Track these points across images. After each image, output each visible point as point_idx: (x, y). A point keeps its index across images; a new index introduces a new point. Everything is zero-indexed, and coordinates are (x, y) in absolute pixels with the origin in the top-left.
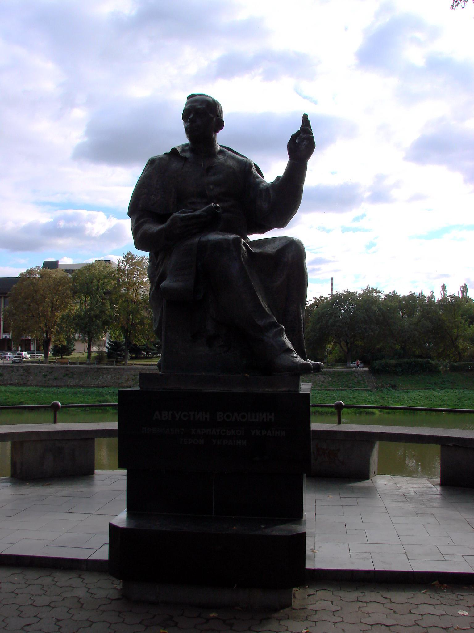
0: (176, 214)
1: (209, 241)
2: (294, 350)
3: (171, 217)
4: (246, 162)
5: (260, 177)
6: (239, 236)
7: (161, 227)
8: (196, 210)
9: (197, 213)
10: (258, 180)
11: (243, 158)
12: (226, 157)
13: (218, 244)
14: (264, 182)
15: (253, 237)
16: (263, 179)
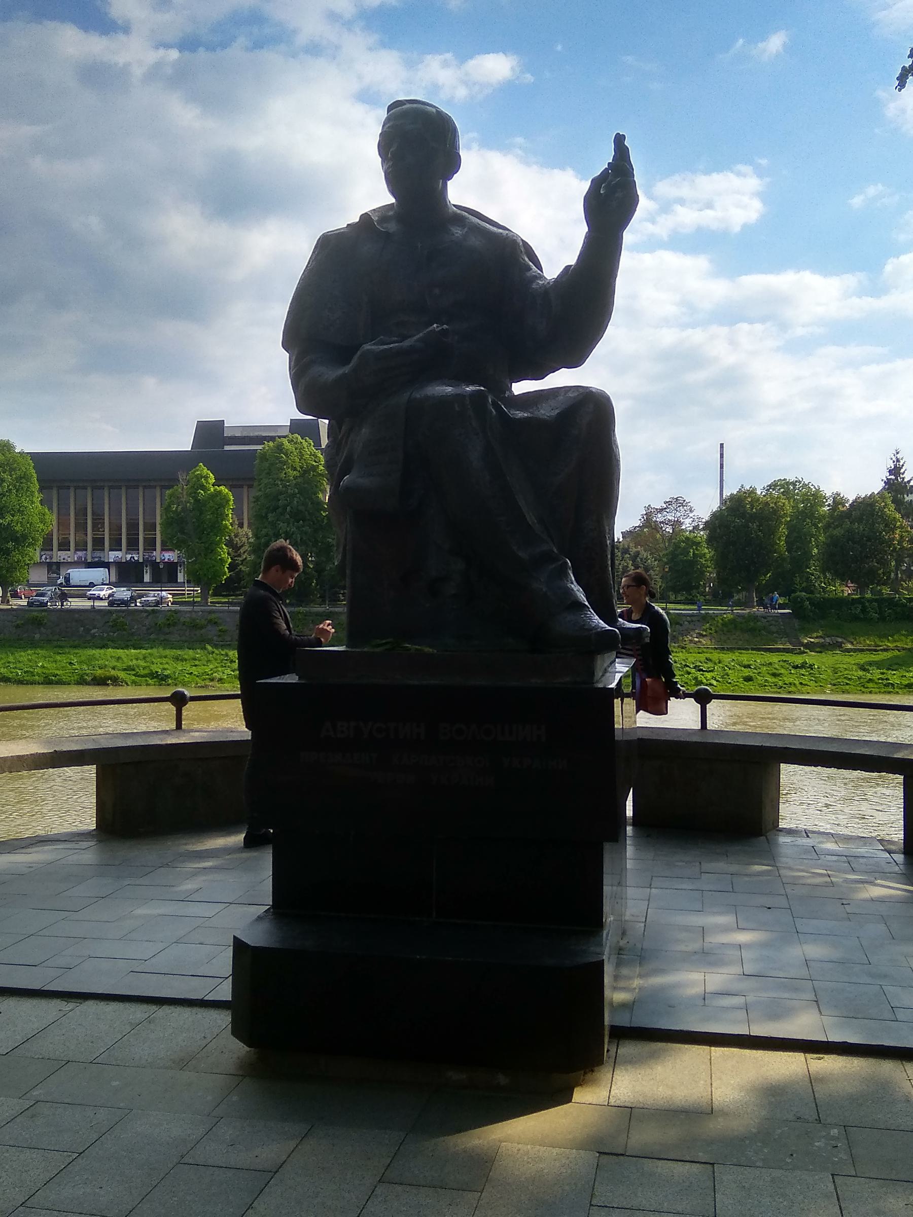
0: (367, 347)
1: (427, 398)
2: (587, 603)
3: (359, 353)
4: (507, 237)
5: (534, 267)
6: (482, 388)
7: (341, 371)
8: (404, 338)
9: (407, 343)
10: (528, 274)
11: (501, 231)
12: (466, 229)
13: (444, 402)
14: (542, 277)
15: (520, 388)
16: (539, 272)
